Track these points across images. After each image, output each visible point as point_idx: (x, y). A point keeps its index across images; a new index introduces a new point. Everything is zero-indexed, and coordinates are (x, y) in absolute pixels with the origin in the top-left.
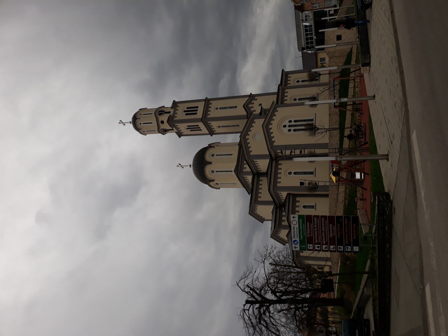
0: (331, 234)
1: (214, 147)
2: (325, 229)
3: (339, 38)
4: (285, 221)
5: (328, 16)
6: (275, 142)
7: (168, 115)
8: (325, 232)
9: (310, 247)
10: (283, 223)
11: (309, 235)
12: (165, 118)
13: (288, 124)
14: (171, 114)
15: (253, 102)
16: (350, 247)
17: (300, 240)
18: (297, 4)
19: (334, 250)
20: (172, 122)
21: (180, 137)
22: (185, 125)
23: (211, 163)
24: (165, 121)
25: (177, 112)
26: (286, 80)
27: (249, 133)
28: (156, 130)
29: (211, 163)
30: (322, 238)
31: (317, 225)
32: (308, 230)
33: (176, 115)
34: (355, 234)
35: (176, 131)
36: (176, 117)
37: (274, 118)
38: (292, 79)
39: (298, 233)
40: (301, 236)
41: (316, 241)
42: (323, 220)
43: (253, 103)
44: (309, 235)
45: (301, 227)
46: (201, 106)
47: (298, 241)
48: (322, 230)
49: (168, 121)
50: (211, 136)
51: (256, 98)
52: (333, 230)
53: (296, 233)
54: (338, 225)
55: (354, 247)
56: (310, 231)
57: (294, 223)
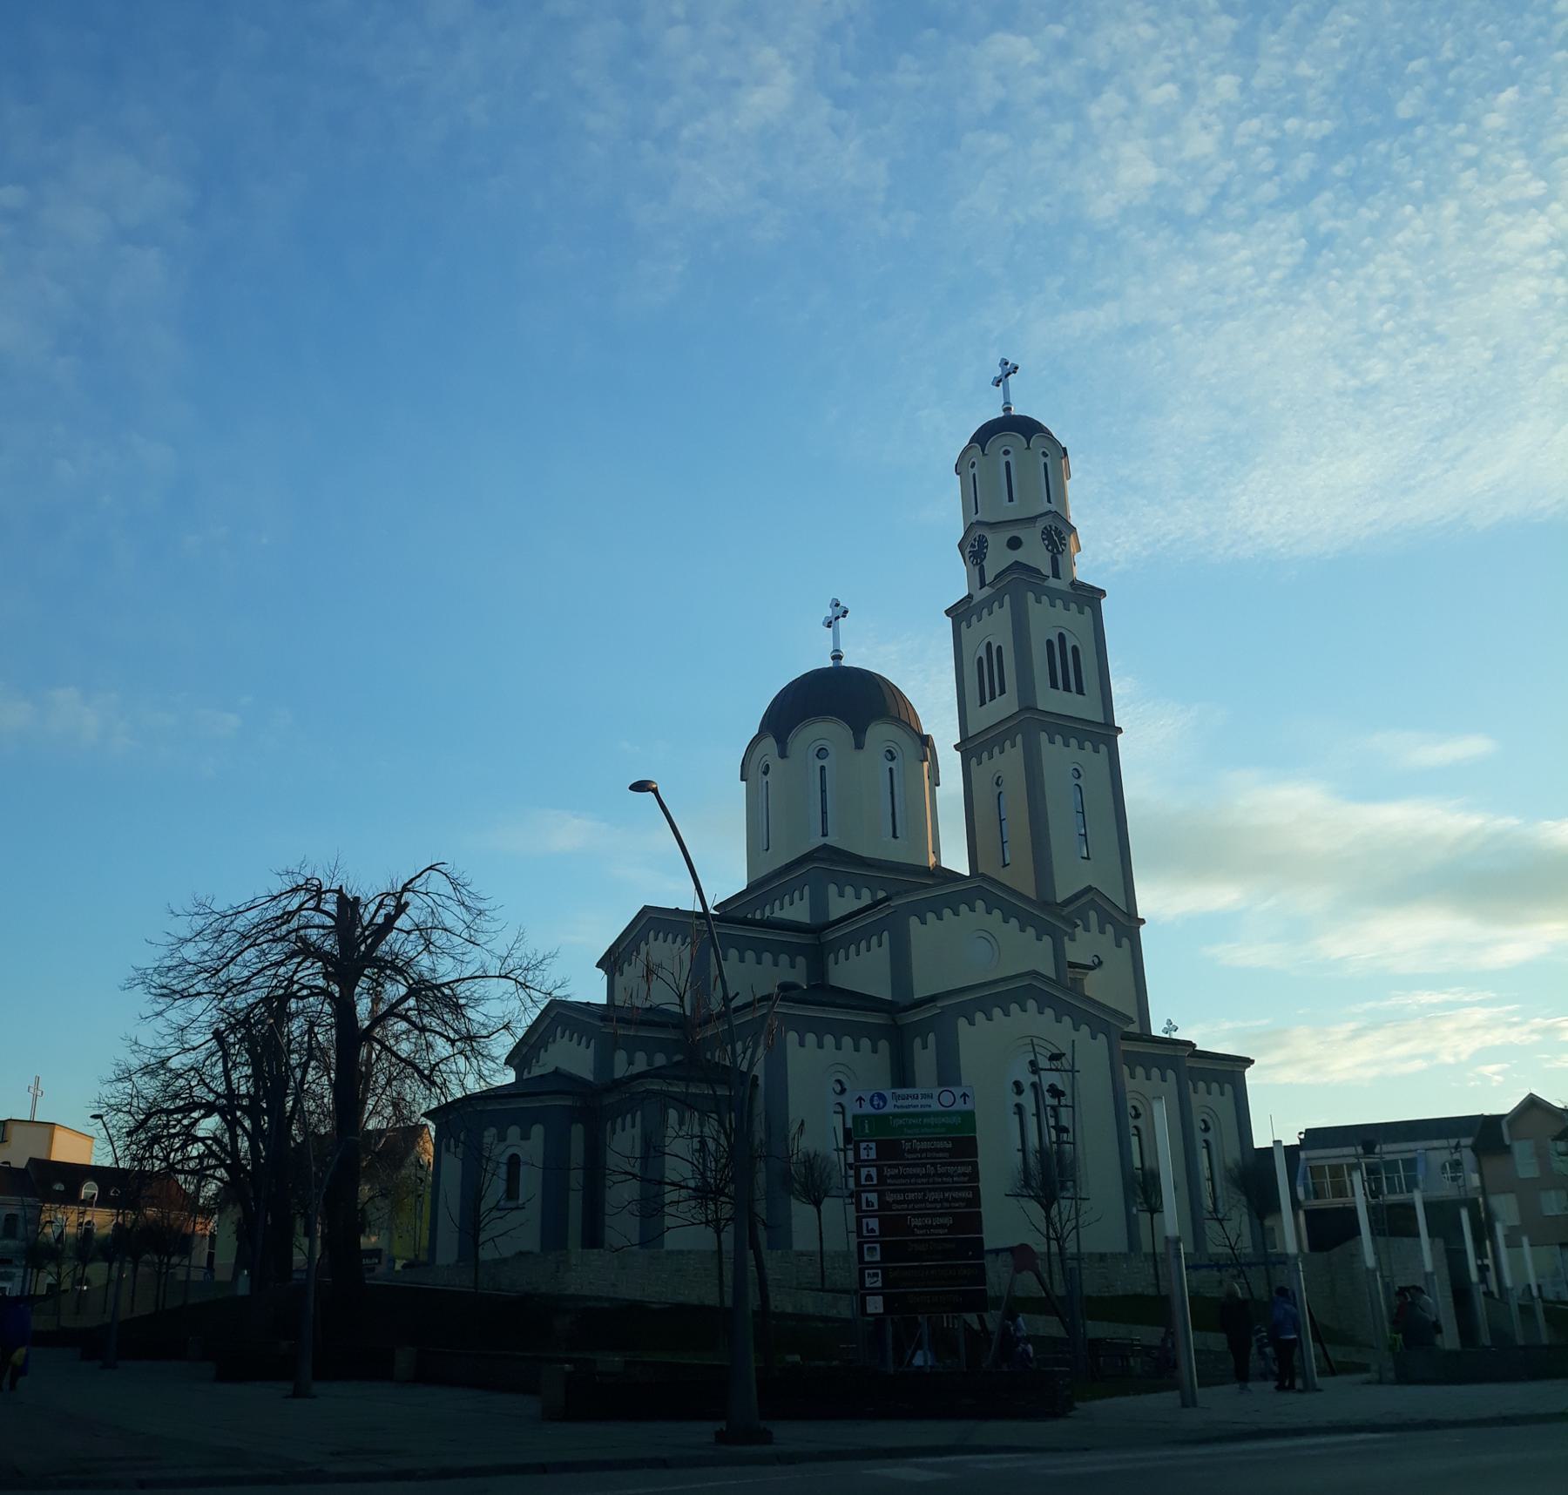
0: (917, 1222)
2: (935, 1201)
4: (631, 1063)
6: (972, 1023)
7: (1047, 570)
8: (923, 1201)
9: (868, 1148)
10: (621, 1057)
12: (1035, 554)
14: (1052, 582)
15: (1109, 928)
16: (879, 1284)
17: (886, 1116)
18: (1509, 1126)
21: (948, 612)
22: (1003, 638)
23: (859, 746)
24: (1018, 555)
25: (1059, 603)
27: (997, 913)
28: (979, 517)
29: (859, 746)
31: (947, 1175)
32: (925, 1145)
36: (1038, 601)
41: (888, 1172)
42: (964, 1194)
43: (1102, 931)
45: (932, 1120)
47: (886, 1110)
48: (931, 1190)
49: (1017, 565)
50: (957, 747)
51: (1125, 942)
52: (931, 1226)
53: (910, 1102)
56: (922, 1151)
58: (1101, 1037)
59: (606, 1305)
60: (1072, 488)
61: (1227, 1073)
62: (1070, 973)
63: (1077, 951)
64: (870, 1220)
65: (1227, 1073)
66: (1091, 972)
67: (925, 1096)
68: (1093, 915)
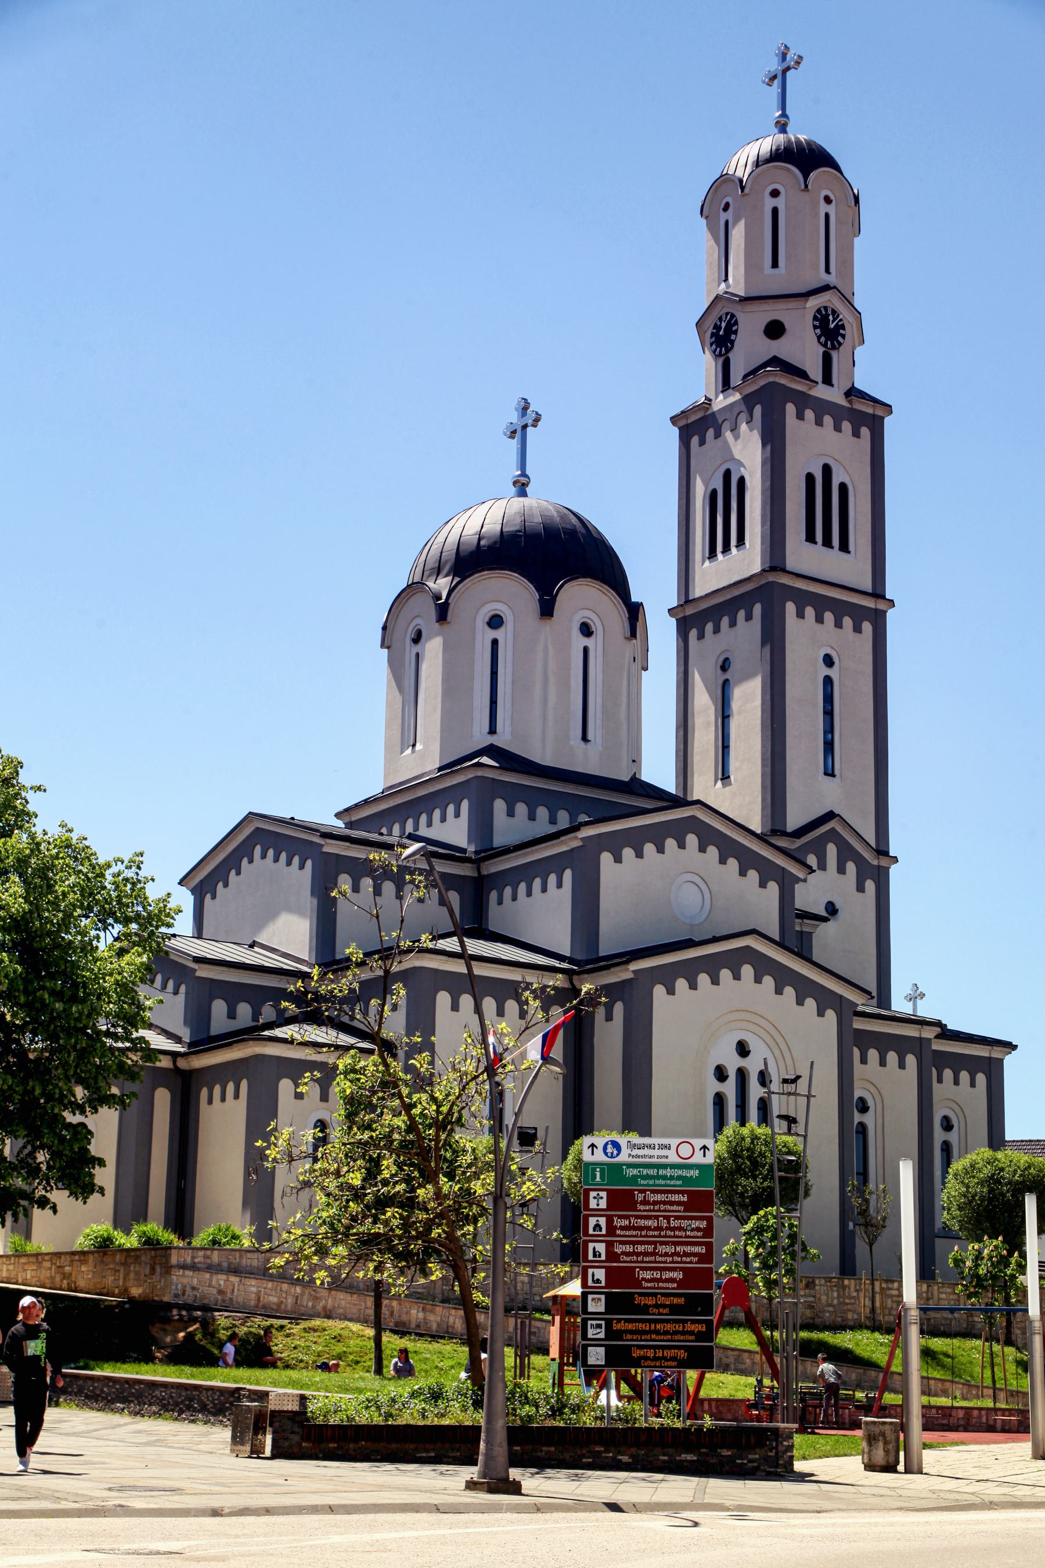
0: (648, 1275)
1: (633, 634)
2: (666, 1254)
4: (232, 1015)
7: (815, 371)
8: (654, 1254)
9: (598, 1198)
10: (219, 1007)
11: (640, 1197)
12: (802, 347)
13: (753, 1065)
14: (821, 392)
15: (851, 867)
16: (602, 1335)
17: (619, 1166)
19: (590, 1283)
20: (773, 398)
21: (674, 420)
23: (547, 610)
25: (828, 420)
26: (958, 1063)
29: (547, 610)
30: (634, 1243)
31: (680, 1229)
32: (659, 1197)
33: (809, 414)
34: (650, 1353)
36: (800, 416)
37: (789, 992)
38: (958, 1096)
39: (647, 1160)
40: (635, 1172)
41: (618, 1223)
42: (697, 1249)
43: (841, 870)
44: (640, 1197)
45: (668, 1172)
46: (849, 568)
48: (662, 1243)
52: (660, 1280)
53: (646, 1152)
54: (681, 1301)
55: (601, 1350)
56: (655, 1203)
59: (620, 1426)
60: (865, 252)
61: (982, 1060)
63: (810, 895)
64: (596, 1271)
66: (823, 924)
67: (663, 1147)
68: (832, 850)
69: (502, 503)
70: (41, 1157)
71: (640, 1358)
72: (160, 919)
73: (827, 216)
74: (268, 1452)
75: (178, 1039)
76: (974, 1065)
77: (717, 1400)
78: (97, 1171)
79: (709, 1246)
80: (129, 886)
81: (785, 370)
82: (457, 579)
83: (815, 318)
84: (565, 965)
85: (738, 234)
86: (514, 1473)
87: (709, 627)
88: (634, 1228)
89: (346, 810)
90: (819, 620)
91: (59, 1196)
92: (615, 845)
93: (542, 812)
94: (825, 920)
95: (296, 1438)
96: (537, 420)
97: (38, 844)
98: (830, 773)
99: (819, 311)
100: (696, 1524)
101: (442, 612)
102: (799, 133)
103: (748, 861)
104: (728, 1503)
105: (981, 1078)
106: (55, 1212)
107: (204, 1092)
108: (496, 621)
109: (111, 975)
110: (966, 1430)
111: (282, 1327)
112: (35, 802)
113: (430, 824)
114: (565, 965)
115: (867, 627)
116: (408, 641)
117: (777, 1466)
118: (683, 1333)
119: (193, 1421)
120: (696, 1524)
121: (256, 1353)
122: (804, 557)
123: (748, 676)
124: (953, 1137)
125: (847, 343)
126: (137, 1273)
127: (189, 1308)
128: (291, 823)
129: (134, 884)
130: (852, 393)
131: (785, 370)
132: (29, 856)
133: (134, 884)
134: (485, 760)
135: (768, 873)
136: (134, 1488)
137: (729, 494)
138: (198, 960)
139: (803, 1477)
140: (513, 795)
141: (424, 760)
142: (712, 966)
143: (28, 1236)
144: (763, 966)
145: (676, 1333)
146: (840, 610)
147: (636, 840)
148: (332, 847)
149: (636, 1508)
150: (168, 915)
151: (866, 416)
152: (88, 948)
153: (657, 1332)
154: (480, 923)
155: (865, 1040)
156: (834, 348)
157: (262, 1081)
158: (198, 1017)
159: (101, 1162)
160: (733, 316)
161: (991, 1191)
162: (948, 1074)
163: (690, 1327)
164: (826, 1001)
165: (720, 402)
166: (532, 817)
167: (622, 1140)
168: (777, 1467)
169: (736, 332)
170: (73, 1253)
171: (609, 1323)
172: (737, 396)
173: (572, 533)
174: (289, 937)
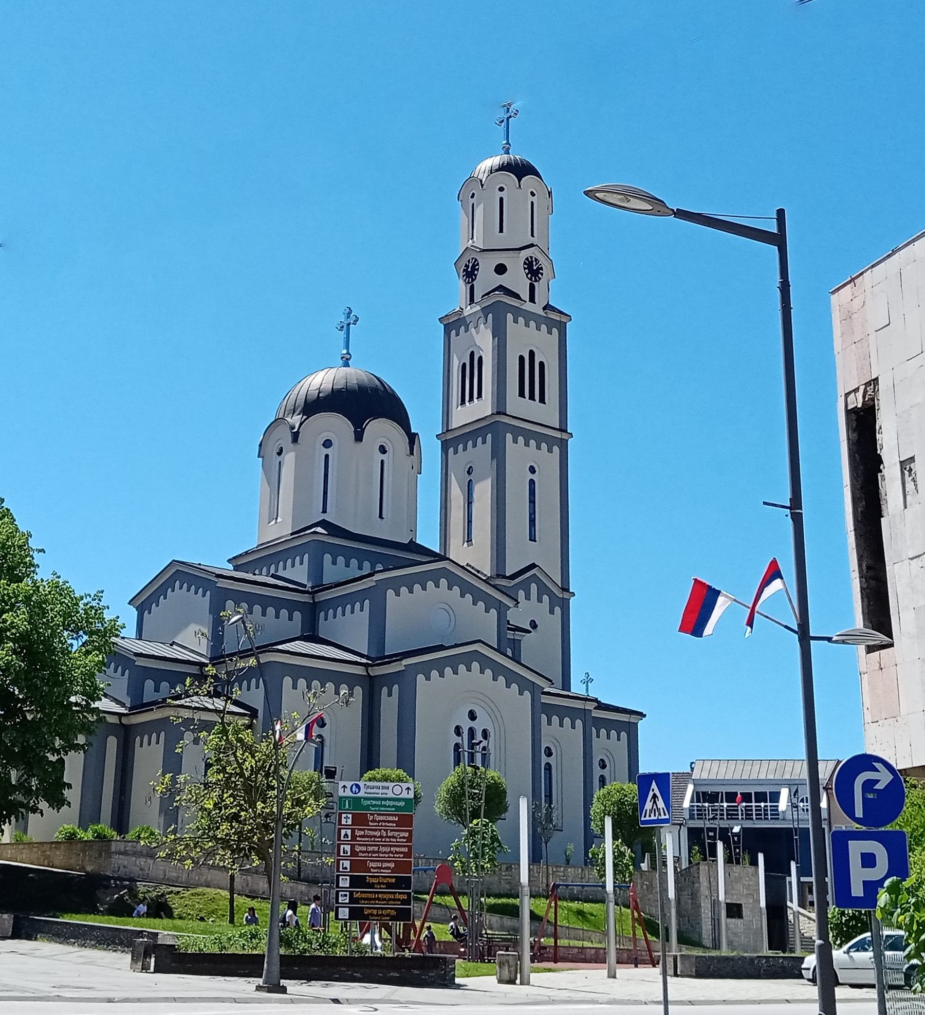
1: (412, 453)
2: (385, 853)
3: (734, 911)
4: (157, 690)
5: (516, 901)
6: (428, 678)
7: (525, 295)
8: (378, 852)
9: (347, 818)
10: (149, 684)
12: (517, 280)
13: (479, 726)
14: (528, 306)
16: (347, 901)
23: (359, 437)
25: (532, 324)
29: (359, 437)
31: (393, 837)
32: (381, 818)
33: (521, 320)
35: (466, 313)
38: (609, 745)
40: (369, 802)
41: (358, 833)
42: (403, 850)
43: (540, 600)
45: (388, 803)
46: (547, 413)
47: (360, 794)
48: (383, 846)
54: (393, 880)
56: (379, 821)
57: (397, 790)
58: (527, 693)
61: (625, 723)
62: (510, 635)
63: (518, 616)
65: (625, 723)
68: (534, 587)
69: (333, 371)
70: (34, 782)
71: (369, 915)
72: (111, 632)
73: (532, 203)
74: (152, 969)
75: (123, 705)
76: (619, 726)
77: (445, 942)
78: (66, 792)
79: (410, 847)
80: (93, 611)
81: (506, 292)
82: (305, 417)
83: (525, 263)
84: (364, 661)
85: (479, 212)
86: (283, 982)
87: (461, 447)
88: (367, 836)
89: (234, 558)
90: (527, 444)
91: (43, 805)
92: (396, 585)
93: (354, 562)
94: (529, 632)
95: (168, 961)
96: (357, 320)
97: (38, 587)
98: (533, 539)
99: (527, 259)
100: (376, 1010)
101: (295, 437)
102: (517, 155)
103: (478, 595)
104: (401, 1000)
105: (624, 735)
106: (42, 815)
107: (138, 739)
108: (327, 444)
109: (78, 669)
110: (596, 962)
111: (178, 892)
112: (38, 558)
113: (285, 569)
114: (364, 661)
115: (556, 449)
116: (275, 453)
117: (445, 980)
118: (394, 900)
119: (115, 951)
120: (376, 1010)
121: (160, 909)
122: (517, 405)
123: (483, 478)
124: (606, 772)
125: (544, 279)
126: (90, 856)
127: (121, 879)
128: (197, 567)
129: (96, 610)
130: (548, 307)
131: (506, 292)
132: (32, 595)
133: (96, 610)
134: (319, 529)
135: (490, 604)
136: (67, 987)
137: (473, 365)
138: (136, 655)
139: (459, 987)
140: (335, 551)
141: (282, 528)
142: (454, 663)
143: (25, 831)
144: (486, 663)
145: (390, 900)
146: (540, 439)
147: (409, 582)
148: (222, 583)
149: (348, 1001)
150: (117, 630)
151: (555, 322)
152: (66, 652)
153: (379, 899)
154: (314, 632)
155: (550, 710)
156: (536, 281)
157: (172, 733)
158: (136, 690)
159: (70, 786)
160: (476, 260)
161: (619, 809)
162: (603, 732)
163: (397, 896)
164: (525, 685)
165: (468, 311)
166: (347, 565)
167: (361, 784)
168: (446, 981)
169: (477, 270)
170: (52, 843)
171: (351, 893)
172: (478, 308)
173: (375, 390)
174: (193, 643)
